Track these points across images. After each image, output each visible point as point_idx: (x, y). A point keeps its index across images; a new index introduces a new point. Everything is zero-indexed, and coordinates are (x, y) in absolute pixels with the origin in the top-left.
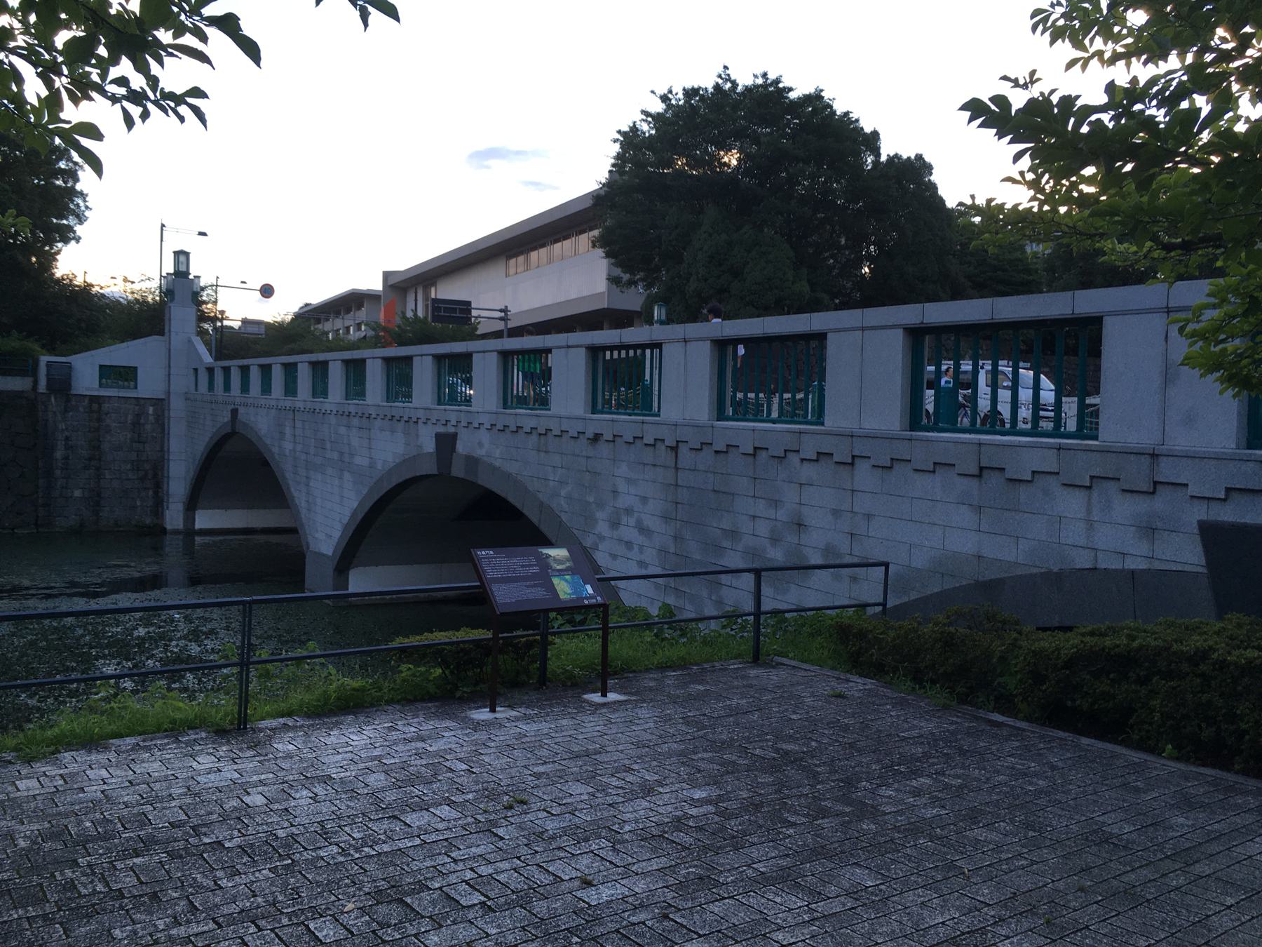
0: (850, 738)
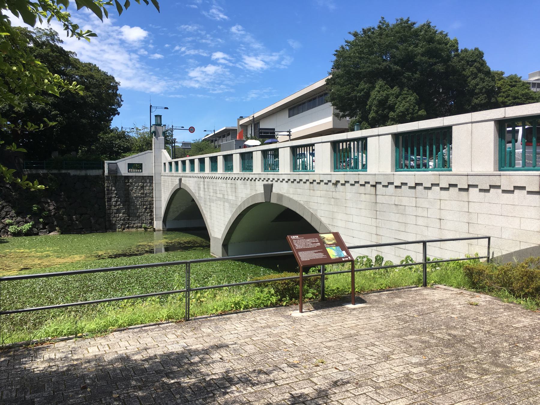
0: (487, 328)
